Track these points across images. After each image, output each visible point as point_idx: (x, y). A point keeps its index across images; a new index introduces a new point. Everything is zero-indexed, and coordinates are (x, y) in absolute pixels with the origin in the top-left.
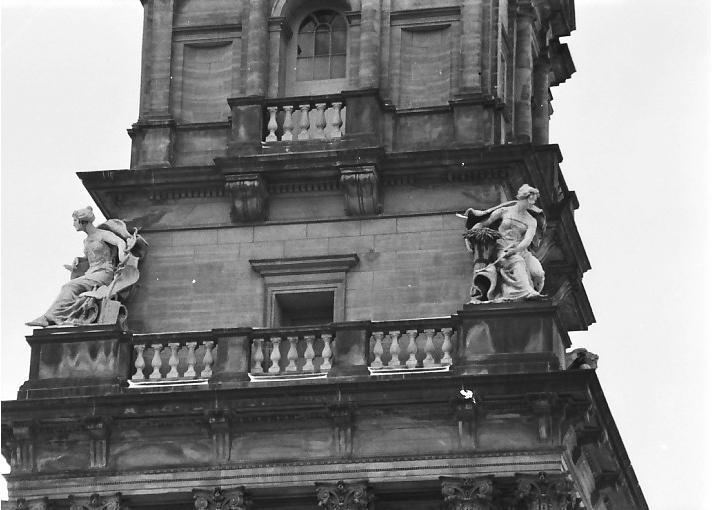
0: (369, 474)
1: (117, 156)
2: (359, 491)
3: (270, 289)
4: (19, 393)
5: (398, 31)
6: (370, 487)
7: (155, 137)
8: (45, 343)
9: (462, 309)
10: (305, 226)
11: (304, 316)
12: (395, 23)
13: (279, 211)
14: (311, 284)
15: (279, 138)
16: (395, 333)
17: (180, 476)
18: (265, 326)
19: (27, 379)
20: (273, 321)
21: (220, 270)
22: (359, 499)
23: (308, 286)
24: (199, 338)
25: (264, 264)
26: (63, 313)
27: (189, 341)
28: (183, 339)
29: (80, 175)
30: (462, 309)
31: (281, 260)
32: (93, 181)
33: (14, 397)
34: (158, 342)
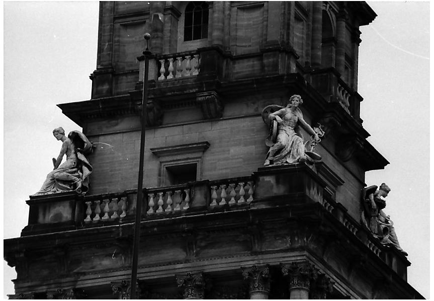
0: (205, 268)
1: (83, 92)
2: (266, 271)
3: (163, 164)
4: (22, 233)
5: (118, 26)
6: (206, 275)
7: (239, 63)
8: (36, 204)
9: (29, 199)
10: (182, 126)
11: (183, 177)
12: (117, 21)
13: (229, 112)
14: (181, 160)
15: (174, 76)
16: (223, 186)
17: (110, 275)
18: (159, 186)
19: (27, 225)
20: (167, 184)
21: (124, 154)
22: (265, 275)
23: (179, 162)
24: (119, 197)
25: (185, 147)
26: (48, 186)
27: (222, 185)
28: (110, 197)
29: (61, 106)
30: (29, 199)
31: (165, 148)
32: (69, 109)
33: (19, 236)
34: (242, 181)
